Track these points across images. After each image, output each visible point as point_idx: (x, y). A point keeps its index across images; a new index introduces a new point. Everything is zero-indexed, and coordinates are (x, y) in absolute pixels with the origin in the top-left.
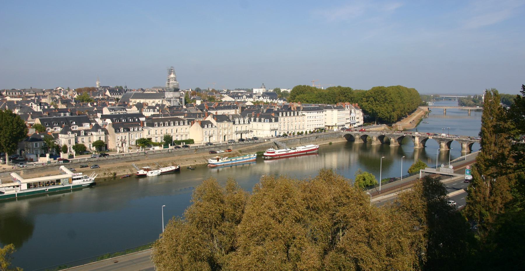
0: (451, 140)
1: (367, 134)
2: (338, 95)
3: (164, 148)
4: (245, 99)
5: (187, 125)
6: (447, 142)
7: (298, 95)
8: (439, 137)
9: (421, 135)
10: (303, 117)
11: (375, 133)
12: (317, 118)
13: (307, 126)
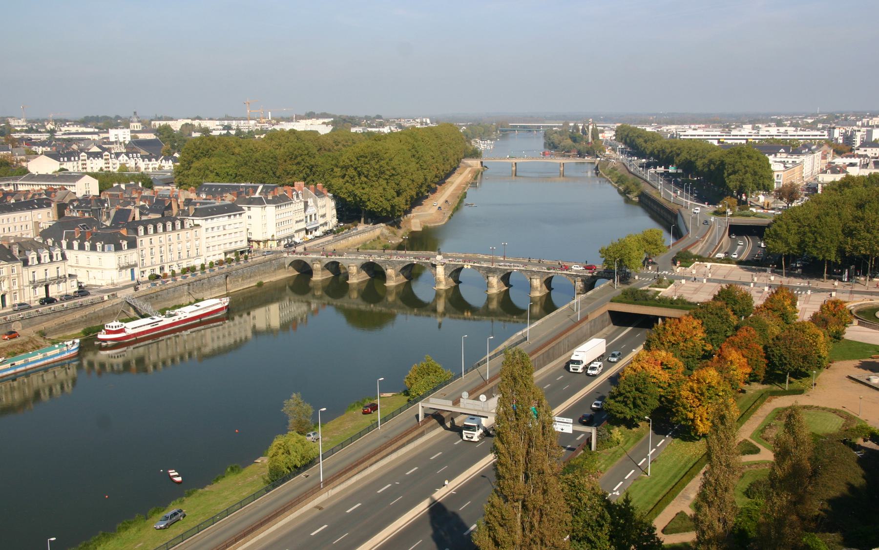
0: (509, 271)
1: (337, 261)
2: (282, 160)
4: (85, 160)
6: (502, 275)
7: (198, 159)
8: (485, 266)
9: (450, 261)
10: (195, 230)
11: (354, 258)
12: (229, 229)
13: (205, 249)
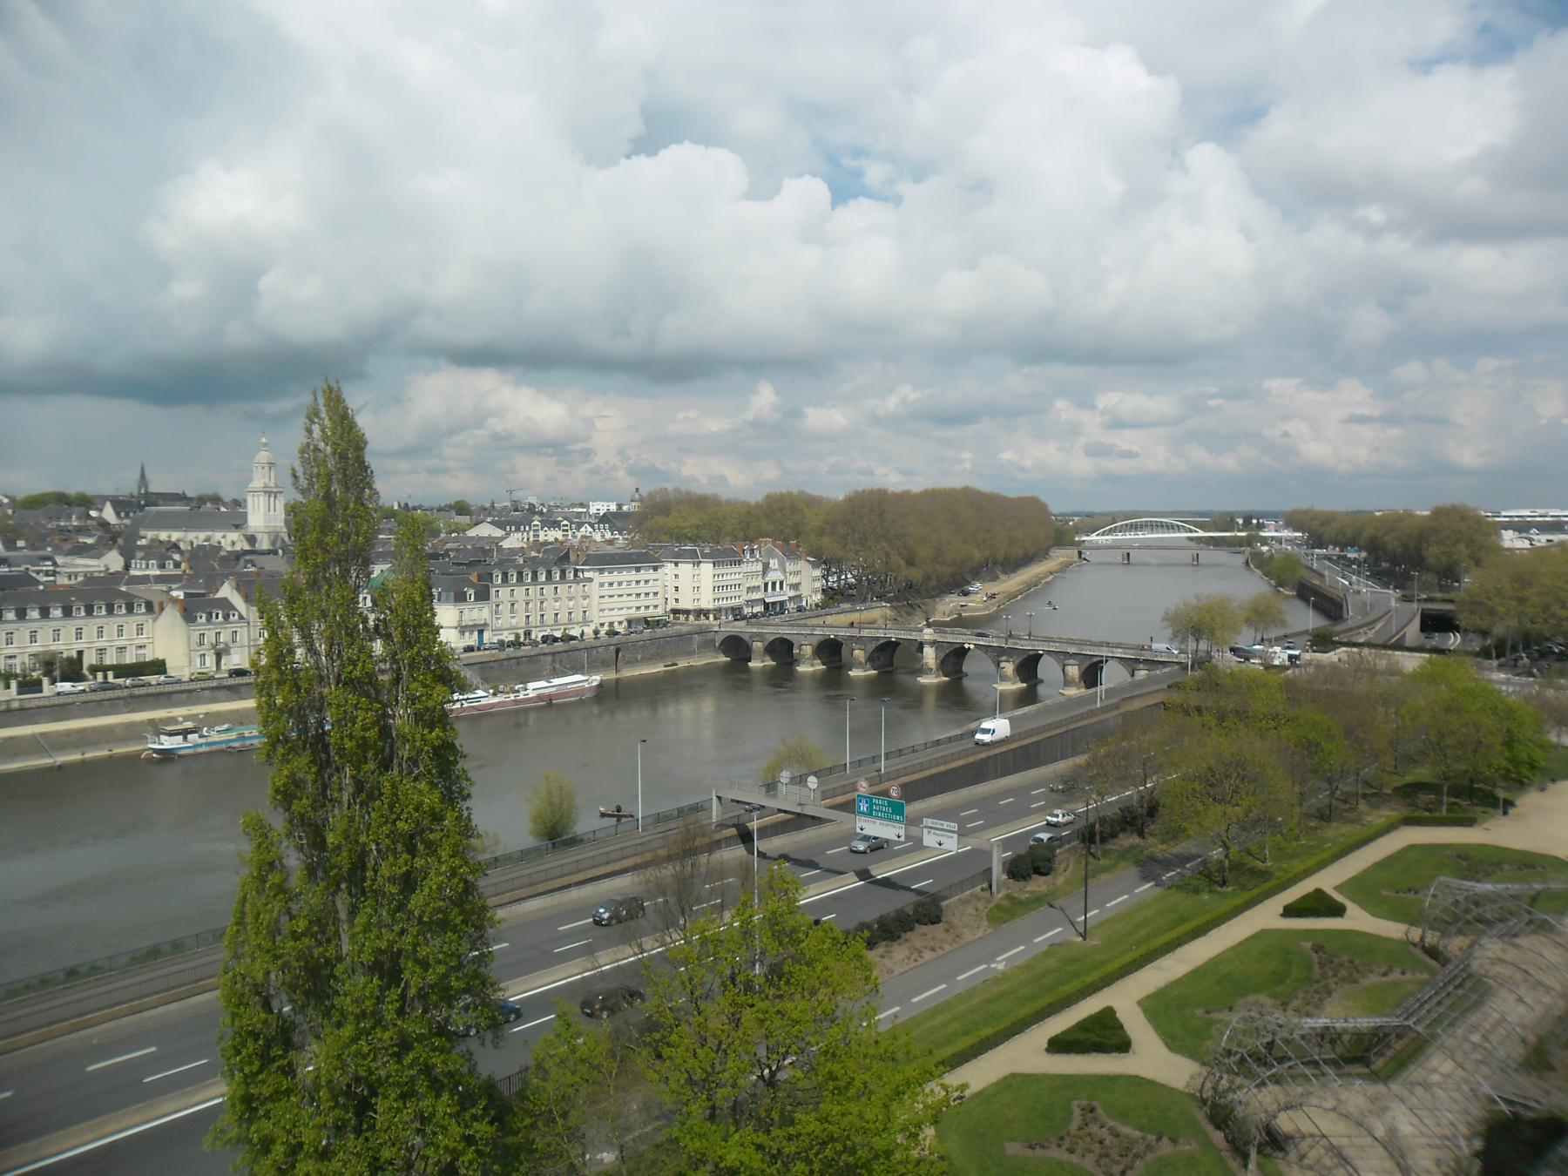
3: (19, 693)
5: (143, 614)
